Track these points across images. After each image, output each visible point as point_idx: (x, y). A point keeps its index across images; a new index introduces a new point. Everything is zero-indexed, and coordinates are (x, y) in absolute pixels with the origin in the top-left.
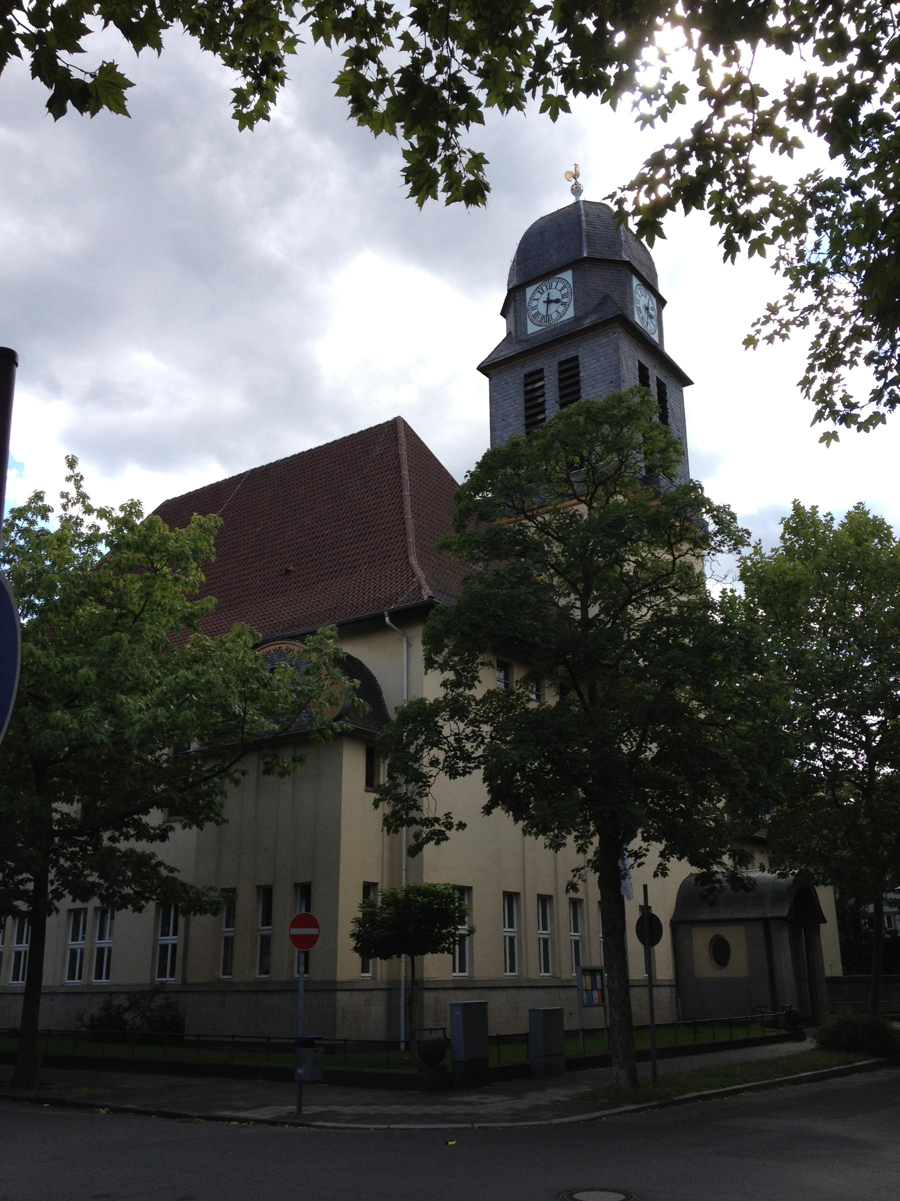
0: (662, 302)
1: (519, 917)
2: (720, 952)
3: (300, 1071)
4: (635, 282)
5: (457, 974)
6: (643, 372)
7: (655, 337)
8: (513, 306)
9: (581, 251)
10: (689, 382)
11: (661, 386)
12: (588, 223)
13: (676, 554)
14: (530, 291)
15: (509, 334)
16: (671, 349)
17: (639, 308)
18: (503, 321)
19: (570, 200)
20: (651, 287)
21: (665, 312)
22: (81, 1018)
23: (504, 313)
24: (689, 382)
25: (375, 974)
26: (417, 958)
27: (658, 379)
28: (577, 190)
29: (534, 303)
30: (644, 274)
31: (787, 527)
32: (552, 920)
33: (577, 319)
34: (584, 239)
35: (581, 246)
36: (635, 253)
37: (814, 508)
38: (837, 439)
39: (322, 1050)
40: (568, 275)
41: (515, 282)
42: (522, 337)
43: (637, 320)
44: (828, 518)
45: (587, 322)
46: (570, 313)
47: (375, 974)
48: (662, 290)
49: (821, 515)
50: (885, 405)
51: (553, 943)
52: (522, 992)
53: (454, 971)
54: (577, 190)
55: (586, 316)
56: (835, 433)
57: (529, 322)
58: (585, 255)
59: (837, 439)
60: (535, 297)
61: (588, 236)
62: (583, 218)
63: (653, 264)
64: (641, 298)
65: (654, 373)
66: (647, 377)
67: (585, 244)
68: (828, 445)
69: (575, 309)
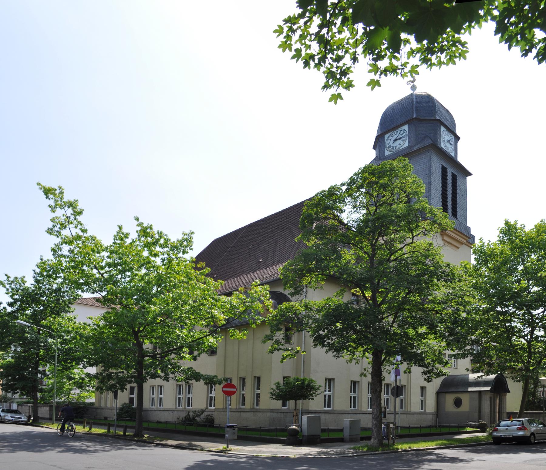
0: (457, 138)
1: (358, 389)
2: (458, 403)
3: (227, 436)
4: (443, 129)
5: (326, 408)
6: (444, 171)
7: (453, 154)
8: (379, 143)
9: (413, 115)
10: (470, 174)
11: (454, 178)
12: (416, 102)
13: (414, 234)
14: (386, 136)
15: (377, 156)
16: (461, 159)
17: (444, 142)
18: (374, 151)
19: (410, 92)
20: (452, 131)
21: (459, 144)
22: (179, 419)
23: (374, 148)
24: (470, 174)
25: (289, 407)
26: (297, 401)
27: (453, 174)
28: (414, 88)
29: (389, 142)
30: (448, 125)
31: (502, 232)
32: (358, 389)
33: (410, 147)
34: (414, 110)
35: (413, 113)
36: (444, 116)
37: (515, 222)
38: (342, 98)
39: (237, 429)
40: (406, 127)
41: (379, 133)
42: (383, 158)
43: (443, 146)
44: (523, 226)
45: (415, 148)
46: (406, 144)
47: (289, 407)
48: (458, 133)
49: (518, 226)
50: (287, 27)
51: (358, 397)
52: (358, 415)
53: (325, 407)
54: (414, 88)
55: (415, 145)
56: (339, 94)
57: (386, 150)
58: (414, 117)
59: (342, 98)
60: (389, 139)
61: (416, 108)
62: (414, 100)
63: (454, 121)
64: (445, 136)
65: (450, 171)
66: (447, 172)
67: (414, 112)
68: (336, 103)
69: (409, 142)
